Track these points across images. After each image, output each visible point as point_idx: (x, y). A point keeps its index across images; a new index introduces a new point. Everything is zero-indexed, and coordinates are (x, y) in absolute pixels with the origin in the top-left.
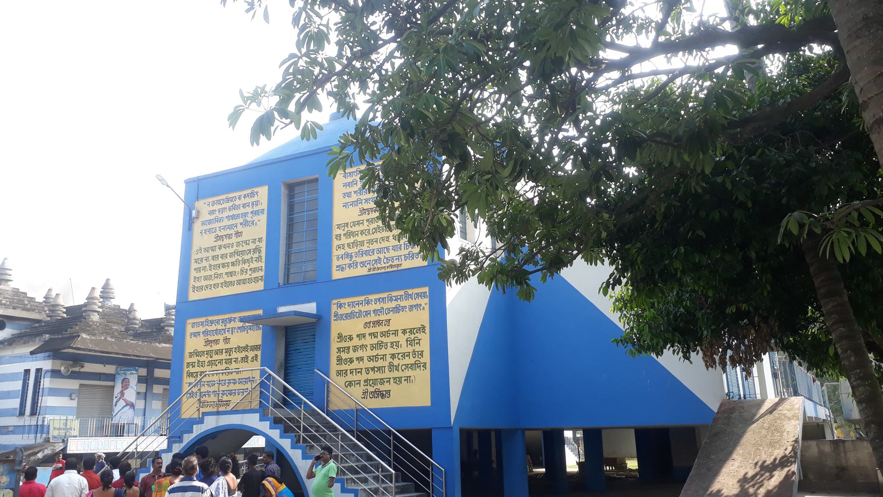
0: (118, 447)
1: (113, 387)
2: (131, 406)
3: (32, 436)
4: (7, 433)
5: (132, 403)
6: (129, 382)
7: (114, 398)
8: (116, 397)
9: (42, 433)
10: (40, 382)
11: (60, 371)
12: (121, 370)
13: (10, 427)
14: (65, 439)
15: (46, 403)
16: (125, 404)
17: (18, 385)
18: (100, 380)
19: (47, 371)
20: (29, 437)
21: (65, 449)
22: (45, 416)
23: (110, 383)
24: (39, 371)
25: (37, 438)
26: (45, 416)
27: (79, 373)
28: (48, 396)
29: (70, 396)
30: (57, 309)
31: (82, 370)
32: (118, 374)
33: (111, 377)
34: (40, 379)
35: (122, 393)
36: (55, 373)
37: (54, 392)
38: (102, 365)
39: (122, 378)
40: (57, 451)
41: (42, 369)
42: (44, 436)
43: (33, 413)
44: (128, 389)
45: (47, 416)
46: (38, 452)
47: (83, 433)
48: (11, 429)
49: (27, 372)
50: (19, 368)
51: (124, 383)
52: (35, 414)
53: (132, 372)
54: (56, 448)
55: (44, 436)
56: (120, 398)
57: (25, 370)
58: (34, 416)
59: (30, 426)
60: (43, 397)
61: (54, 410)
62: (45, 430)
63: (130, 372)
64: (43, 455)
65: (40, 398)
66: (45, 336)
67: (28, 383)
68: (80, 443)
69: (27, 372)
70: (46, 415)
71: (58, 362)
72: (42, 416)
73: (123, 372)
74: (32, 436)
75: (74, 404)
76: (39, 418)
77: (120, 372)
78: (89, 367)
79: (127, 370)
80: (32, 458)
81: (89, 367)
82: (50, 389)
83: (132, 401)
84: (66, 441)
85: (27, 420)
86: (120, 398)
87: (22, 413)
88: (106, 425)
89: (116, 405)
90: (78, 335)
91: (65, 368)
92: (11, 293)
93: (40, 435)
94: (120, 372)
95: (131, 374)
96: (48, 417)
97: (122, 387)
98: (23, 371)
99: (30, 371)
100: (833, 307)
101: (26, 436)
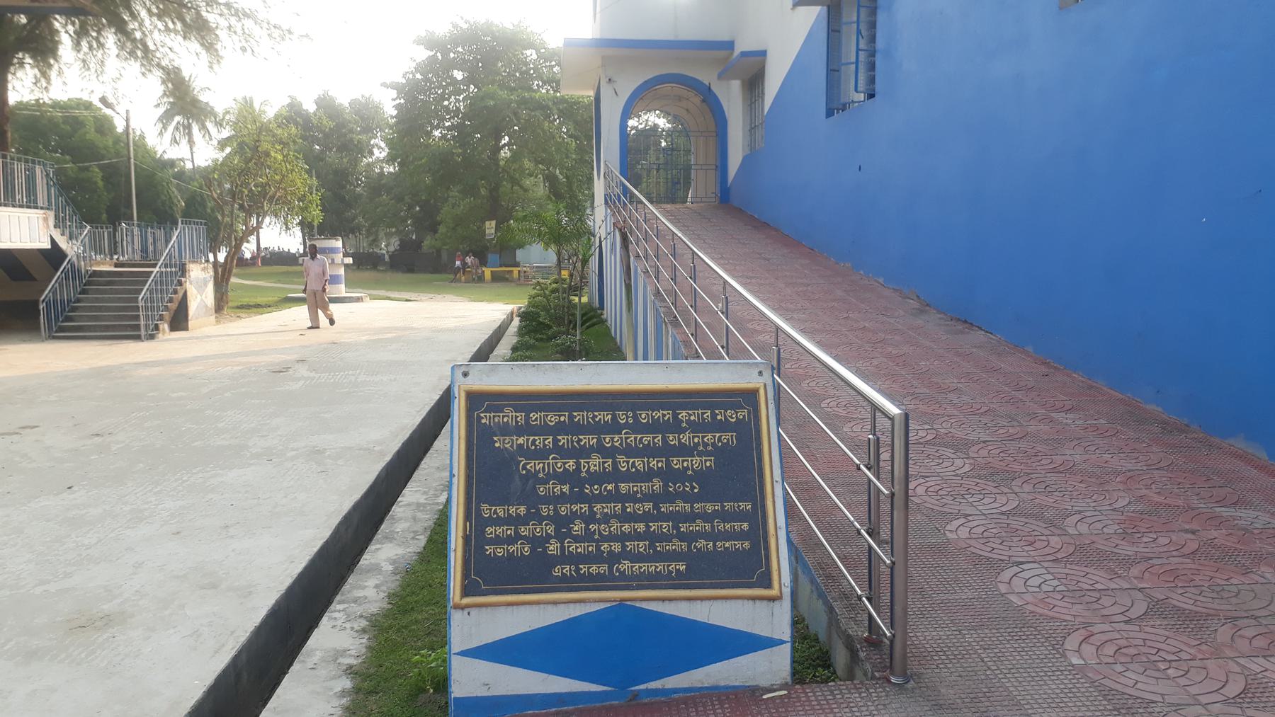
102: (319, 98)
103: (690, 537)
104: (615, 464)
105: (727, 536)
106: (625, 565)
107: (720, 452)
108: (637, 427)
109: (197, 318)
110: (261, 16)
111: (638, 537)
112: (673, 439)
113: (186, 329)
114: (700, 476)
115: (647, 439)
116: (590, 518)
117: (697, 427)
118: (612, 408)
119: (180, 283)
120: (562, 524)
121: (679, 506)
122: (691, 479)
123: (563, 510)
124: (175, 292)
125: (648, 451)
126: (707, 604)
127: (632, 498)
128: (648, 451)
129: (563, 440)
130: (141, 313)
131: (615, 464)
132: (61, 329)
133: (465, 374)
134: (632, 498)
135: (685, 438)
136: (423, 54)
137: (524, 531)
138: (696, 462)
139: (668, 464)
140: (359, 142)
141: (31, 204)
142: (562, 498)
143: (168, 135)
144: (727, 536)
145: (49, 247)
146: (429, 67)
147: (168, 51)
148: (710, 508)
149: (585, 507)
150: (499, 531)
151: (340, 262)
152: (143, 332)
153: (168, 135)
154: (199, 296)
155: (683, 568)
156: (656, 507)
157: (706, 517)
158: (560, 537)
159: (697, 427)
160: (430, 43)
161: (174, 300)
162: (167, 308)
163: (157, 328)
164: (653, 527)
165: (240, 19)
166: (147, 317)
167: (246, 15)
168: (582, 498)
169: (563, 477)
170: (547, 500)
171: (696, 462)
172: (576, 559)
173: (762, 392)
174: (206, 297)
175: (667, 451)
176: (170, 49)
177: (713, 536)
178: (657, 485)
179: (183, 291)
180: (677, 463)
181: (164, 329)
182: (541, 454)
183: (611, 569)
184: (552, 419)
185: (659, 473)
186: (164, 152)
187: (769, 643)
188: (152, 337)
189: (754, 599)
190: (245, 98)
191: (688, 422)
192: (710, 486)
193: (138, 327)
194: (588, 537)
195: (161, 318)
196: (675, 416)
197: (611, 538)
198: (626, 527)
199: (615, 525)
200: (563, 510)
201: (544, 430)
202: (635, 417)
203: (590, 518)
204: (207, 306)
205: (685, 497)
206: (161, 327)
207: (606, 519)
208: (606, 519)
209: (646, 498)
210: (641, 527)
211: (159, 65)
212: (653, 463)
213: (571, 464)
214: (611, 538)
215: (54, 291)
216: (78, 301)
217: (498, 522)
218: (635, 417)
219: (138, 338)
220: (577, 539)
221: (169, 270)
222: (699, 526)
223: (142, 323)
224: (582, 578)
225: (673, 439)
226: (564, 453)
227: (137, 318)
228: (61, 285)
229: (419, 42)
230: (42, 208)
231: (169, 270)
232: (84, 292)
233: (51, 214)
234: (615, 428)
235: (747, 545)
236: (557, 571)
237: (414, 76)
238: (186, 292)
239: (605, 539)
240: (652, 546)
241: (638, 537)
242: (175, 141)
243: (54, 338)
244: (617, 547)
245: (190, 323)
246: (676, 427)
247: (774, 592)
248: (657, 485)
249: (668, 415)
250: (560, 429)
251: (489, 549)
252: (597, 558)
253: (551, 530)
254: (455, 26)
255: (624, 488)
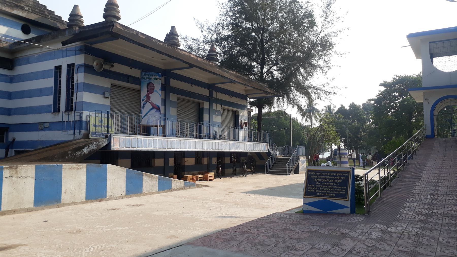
0: (155, 146)
1: (139, 91)
2: (157, 109)
3: (71, 132)
4: (44, 129)
5: (159, 107)
6: (153, 86)
7: (141, 101)
8: (143, 100)
9: (80, 128)
10: (73, 79)
11: (93, 67)
12: (145, 75)
13: (45, 124)
14: (109, 135)
15: (82, 98)
16: (151, 107)
17: (50, 83)
18: (128, 82)
19: (80, 66)
20: (68, 132)
21: (109, 144)
22: (81, 112)
23: (136, 87)
24: (70, 67)
25: (76, 134)
26: (81, 112)
27: (110, 71)
28: (83, 91)
29: (104, 94)
30: (77, 18)
31: (112, 69)
32: (143, 78)
33: (137, 81)
34: (73, 75)
35: (148, 97)
36: (88, 69)
37: (89, 88)
38: (129, 68)
39: (147, 83)
40: (102, 146)
41: (74, 64)
42: (83, 132)
43: (69, 108)
44: (153, 93)
45: (83, 112)
46: (83, 147)
47: (123, 131)
48: (47, 125)
49: (58, 68)
50: (50, 65)
51: (149, 87)
52: (72, 110)
53: (156, 77)
54: (100, 143)
55: (83, 132)
56: (147, 101)
57: (56, 67)
58: (70, 113)
59: (68, 122)
60: (78, 93)
61: (91, 107)
62: (84, 125)
63: (154, 77)
64: (88, 150)
65: (75, 94)
66: (75, 28)
67: (60, 81)
68: (122, 139)
69: (58, 68)
70: (83, 110)
71: (90, 57)
72: (79, 112)
73: (147, 76)
74: (71, 132)
75: (107, 102)
76: (76, 114)
77: (144, 76)
78: (119, 68)
79: (151, 75)
80: (78, 153)
81: (119, 68)
82: (85, 84)
83: (158, 105)
84: (109, 137)
85: (61, 117)
86: (147, 101)
87: (56, 109)
88: (130, 127)
89: (143, 108)
90: (112, 24)
91: (97, 64)
92: (32, 3)
93: (78, 131)
94: (144, 76)
95: (155, 79)
96: (85, 114)
97: (148, 91)
98: (53, 68)
99: (61, 69)
100: (280, 119)
101: (65, 132)
102: (351, 105)
103: (336, 191)
104: (327, 180)
105: (342, 191)
106: (326, 194)
107: (343, 180)
108: (331, 176)
109: (301, 171)
110: (322, 89)
111: (329, 190)
112: (336, 178)
113: (298, 173)
114: (339, 183)
115: (332, 177)
116: (322, 187)
117: (339, 176)
118: (328, 173)
119: (297, 161)
120: (319, 188)
121: (335, 187)
122: (338, 183)
123: (319, 186)
124: (296, 164)
125: (332, 179)
126: (339, 200)
127: (329, 185)
128: (332, 179)
129: (320, 177)
130: (287, 169)
131: (327, 180)
132: (269, 172)
133: (308, 167)
134: (329, 185)
135: (338, 178)
136: (383, 89)
137: (313, 188)
138: (339, 181)
139: (335, 181)
140: (363, 118)
141: (265, 142)
142: (319, 184)
143: (305, 119)
144: (342, 191)
145: (268, 152)
146: (384, 93)
147: (299, 101)
148: (340, 187)
149: (322, 186)
150: (310, 188)
151: (347, 157)
152: (287, 173)
153: (305, 119)
154: (302, 165)
155: (335, 195)
156: (332, 187)
157: (339, 189)
158: (318, 190)
159: (339, 176)
160: (384, 84)
161: (296, 166)
162: (293, 168)
163: (291, 173)
164: (331, 189)
165: (317, 91)
166: (288, 170)
167: (319, 90)
168: (322, 185)
169: (319, 182)
170: (317, 185)
171: (339, 181)
172: (320, 193)
173: (350, 172)
174: (304, 165)
175: (335, 179)
176: (299, 100)
177: (340, 191)
178: (333, 184)
179: (298, 163)
180: (336, 181)
181: (292, 173)
182: (317, 178)
183: (324, 194)
184: (319, 174)
185: (333, 182)
186: (303, 124)
187: (347, 207)
188: (289, 175)
189: (344, 200)
190: (328, 106)
191: (339, 175)
192: (340, 184)
193: (286, 172)
194: (322, 190)
195: (292, 170)
196: (337, 174)
197: (325, 190)
198: (327, 189)
199: (326, 189)
200: (319, 186)
201: (318, 175)
202: (331, 174)
203: (322, 187)
204: (304, 168)
205: (336, 186)
206: (292, 172)
207: (325, 188)
208: (325, 188)
209: (331, 185)
210: (329, 189)
211: (296, 104)
212: (332, 181)
213: (321, 180)
214: (325, 190)
215: (268, 162)
216: (273, 165)
217: (310, 187)
218: (331, 174)
219: (286, 175)
220: (320, 190)
221: (294, 158)
222: (338, 190)
223: (287, 171)
224: (321, 195)
225: (336, 178)
226: (320, 178)
227: (286, 170)
228: (270, 161)
229: (381, 85)
230: (267, 143)
231: (294, 158)
232: (275, 163)
233: (268, 144)
234: (328, 175)
235: (344, 193)
236: (317, 194)
237: (380, 96)
238: (299, 163)
239: (324, 190)
240: (331, 192)
241: (329, 190)
242: (306, 120)
243: (268, 174)
244: (326, 192)
245: (299, 172)
246: (337, 176)
247: (347, 200)
248: (333, 184)
249: (336, 174)
250: (320, 175)
251: (309, 190)
252: (323, 193)
253: (317, 188)
254: (394, 78)
255: (328, 184)
